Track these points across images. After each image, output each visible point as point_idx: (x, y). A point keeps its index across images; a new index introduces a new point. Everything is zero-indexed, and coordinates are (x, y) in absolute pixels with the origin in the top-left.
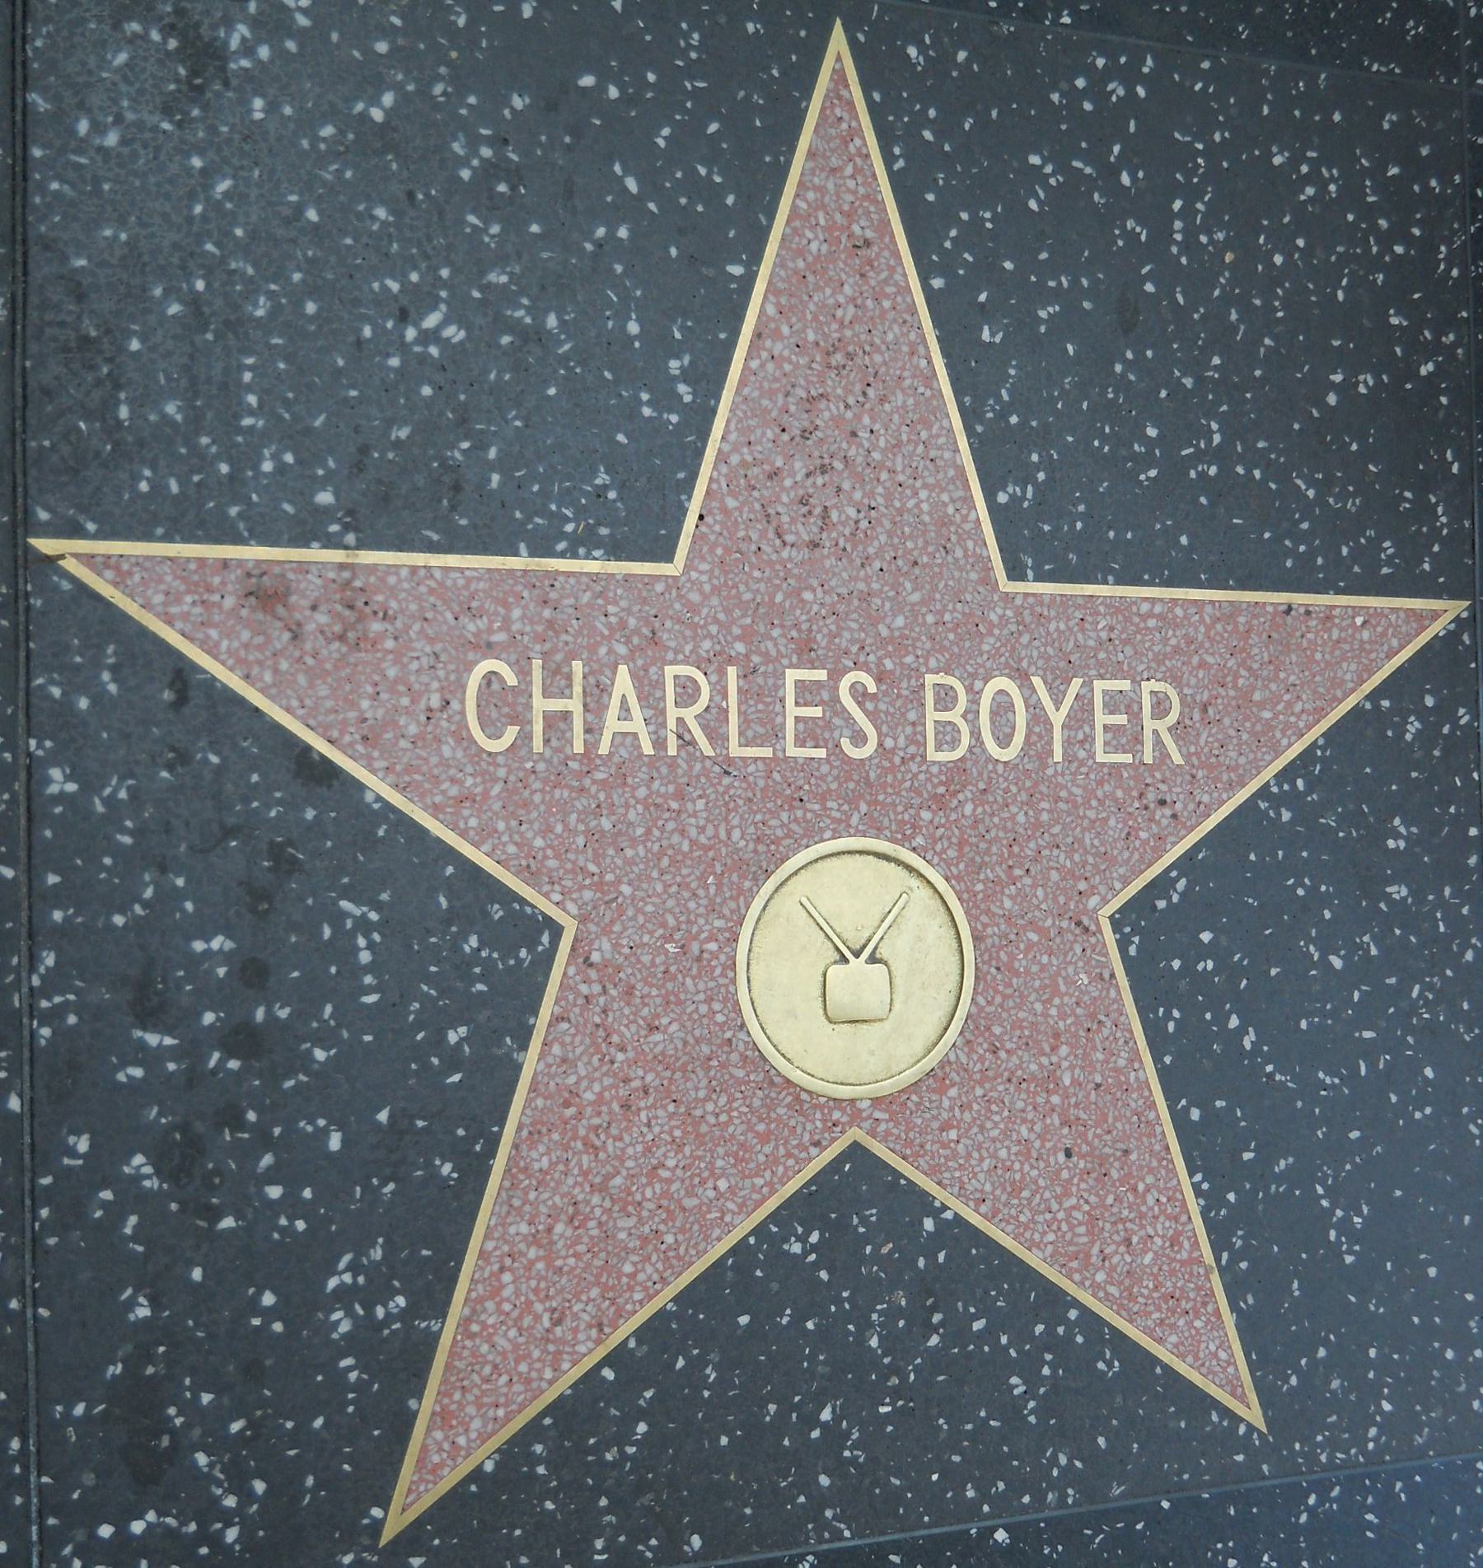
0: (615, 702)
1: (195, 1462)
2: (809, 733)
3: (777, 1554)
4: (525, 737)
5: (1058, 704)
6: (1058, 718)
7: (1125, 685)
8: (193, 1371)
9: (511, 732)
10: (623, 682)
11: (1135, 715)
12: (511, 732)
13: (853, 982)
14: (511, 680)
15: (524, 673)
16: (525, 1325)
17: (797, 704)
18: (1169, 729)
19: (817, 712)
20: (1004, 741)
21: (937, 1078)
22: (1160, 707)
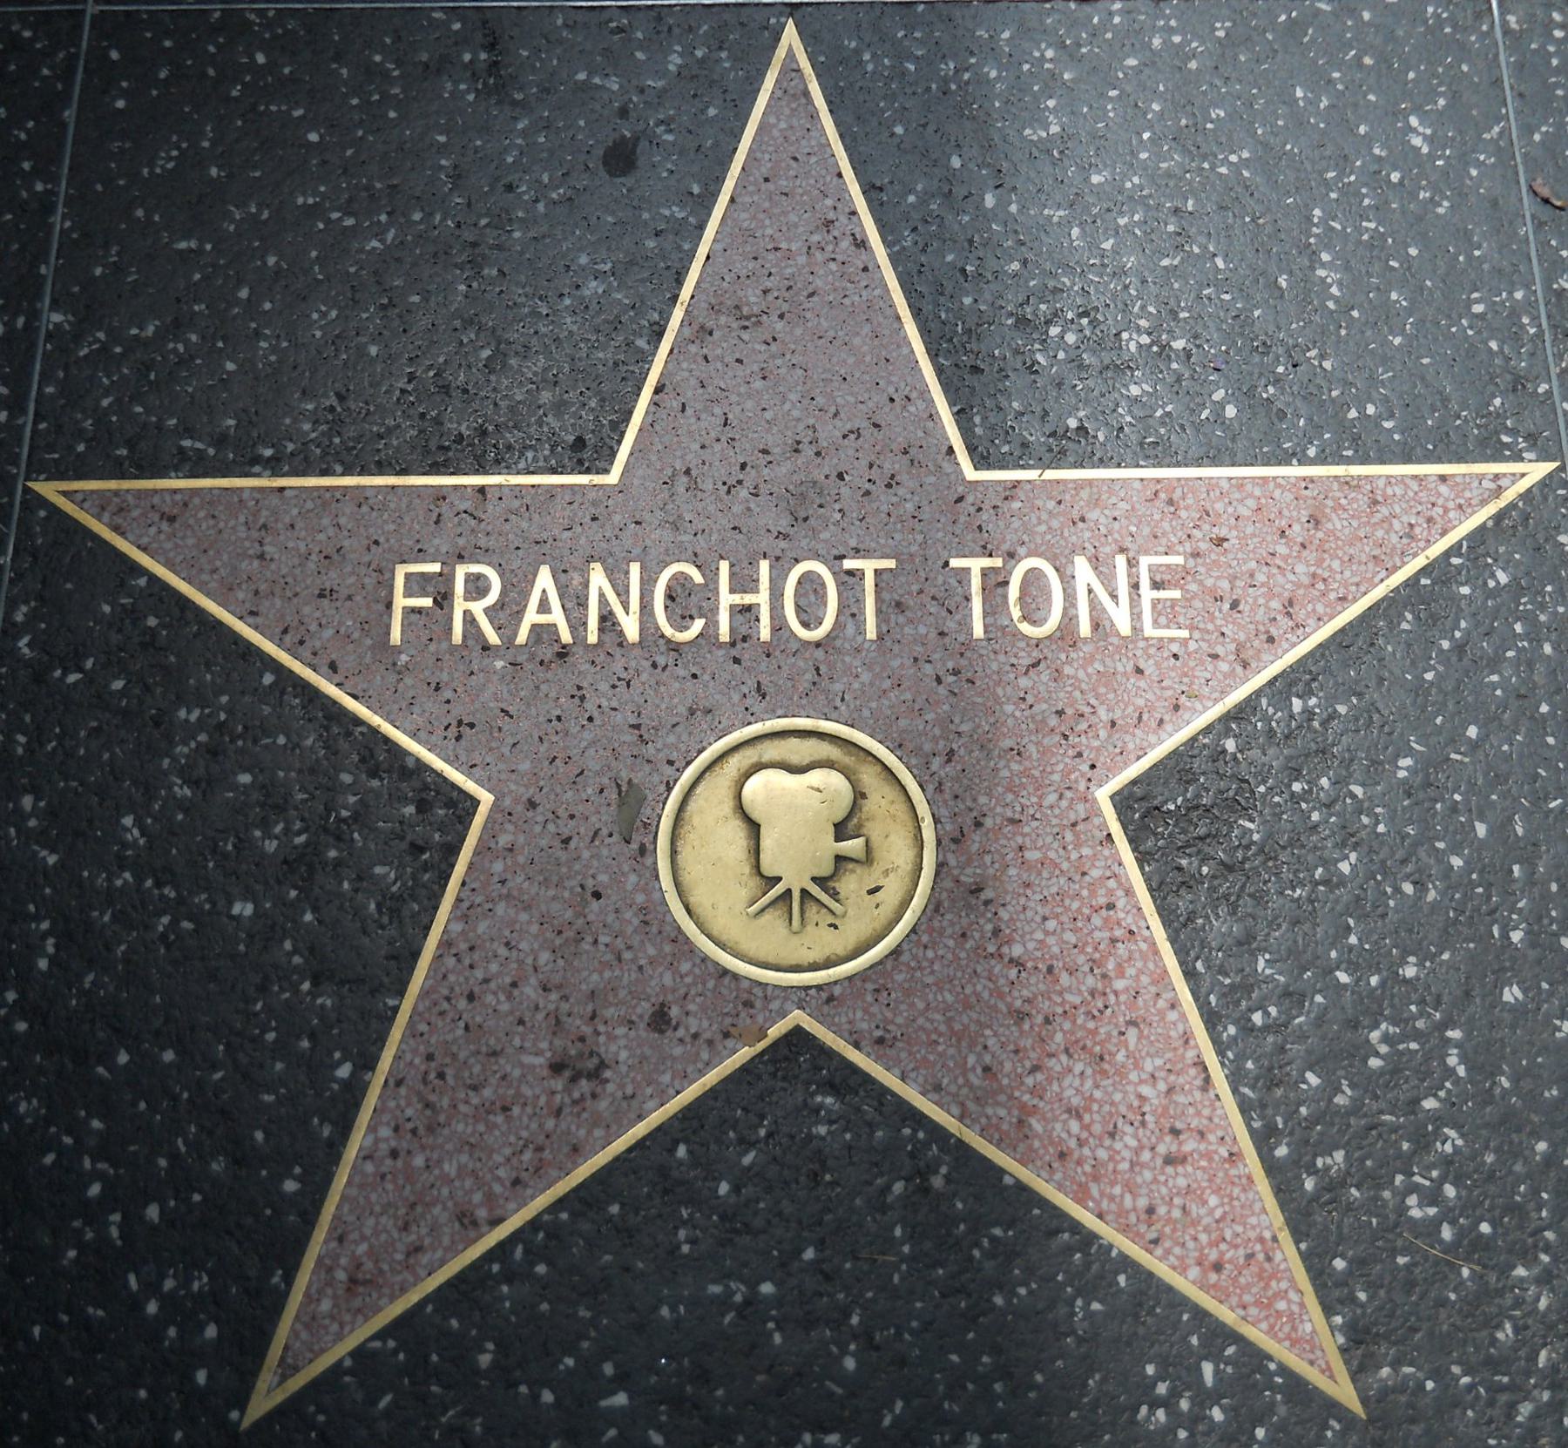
1: (951, 1361)
4: (712, 624)
9: (698, 625)
10: (544, 579)
12: (698, 625)
14: (698, 577)
15: (711, 576)
16: (404, 1215)
17: (732, 591)
19: (427, 602)
20: (810, 584)
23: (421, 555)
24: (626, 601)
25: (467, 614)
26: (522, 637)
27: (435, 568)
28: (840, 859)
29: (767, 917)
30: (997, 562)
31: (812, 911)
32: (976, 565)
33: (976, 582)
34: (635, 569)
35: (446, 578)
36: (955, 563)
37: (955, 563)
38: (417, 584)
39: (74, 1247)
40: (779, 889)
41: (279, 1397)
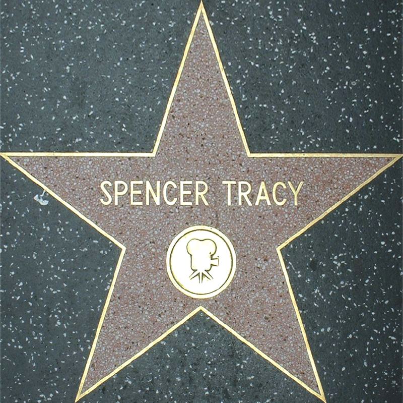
2: (186, 198)
6: (296, 194)
7: (191, 182)
8: (365, 296)
9: (175, 200)
11: (193, 192)
12: (175, 200)
13: (201, 264)
18: (184, 195)
21: (232, 288)
22: (202, 188)
23: (138, 178)
24: (155, 193)
25: (242, 196)
26: (257, 204)
27: (191, 182)
28: (212, 265)
30: (234, 183)
31: (205, 278)
32: (229, 183)
33: (229, 187)
34: (158, 183)
35: (194, 185)
38: (136, 187)
40: (196, 273)
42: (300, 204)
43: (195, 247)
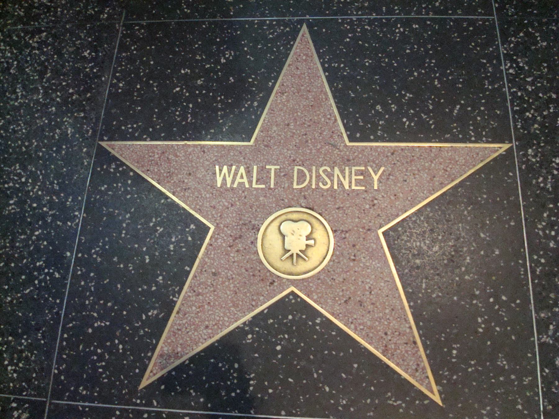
0: (239, 175)
3: (64, 310)
5: (376, 175)
6: (376, 178)
10: (242, 170)
13: (296, 246)
17: (355, 175)
26: (235, 186)
28: (307, 246)
29: (308, 255)
31: (301, 261)
32: (273, 168)
36: (267, 167)
37: (267, 167)
39: (468, 372)
40: (290, 253)
41: (435, 388)
42: (295, 191)
43: (286, 227)
